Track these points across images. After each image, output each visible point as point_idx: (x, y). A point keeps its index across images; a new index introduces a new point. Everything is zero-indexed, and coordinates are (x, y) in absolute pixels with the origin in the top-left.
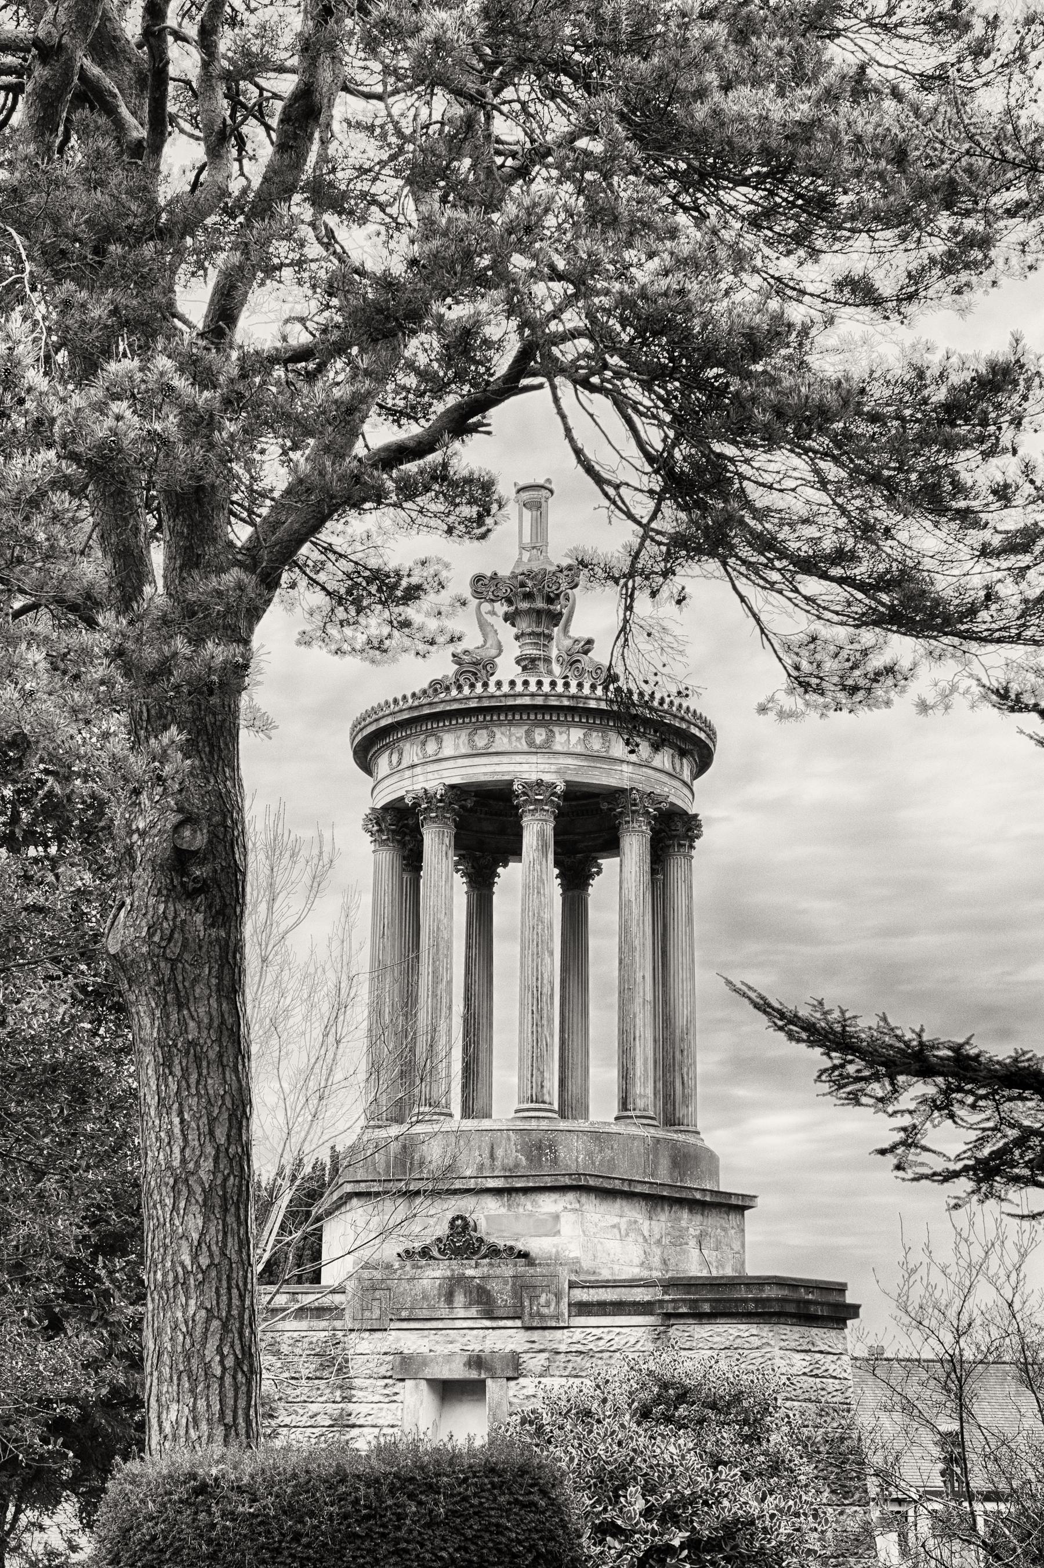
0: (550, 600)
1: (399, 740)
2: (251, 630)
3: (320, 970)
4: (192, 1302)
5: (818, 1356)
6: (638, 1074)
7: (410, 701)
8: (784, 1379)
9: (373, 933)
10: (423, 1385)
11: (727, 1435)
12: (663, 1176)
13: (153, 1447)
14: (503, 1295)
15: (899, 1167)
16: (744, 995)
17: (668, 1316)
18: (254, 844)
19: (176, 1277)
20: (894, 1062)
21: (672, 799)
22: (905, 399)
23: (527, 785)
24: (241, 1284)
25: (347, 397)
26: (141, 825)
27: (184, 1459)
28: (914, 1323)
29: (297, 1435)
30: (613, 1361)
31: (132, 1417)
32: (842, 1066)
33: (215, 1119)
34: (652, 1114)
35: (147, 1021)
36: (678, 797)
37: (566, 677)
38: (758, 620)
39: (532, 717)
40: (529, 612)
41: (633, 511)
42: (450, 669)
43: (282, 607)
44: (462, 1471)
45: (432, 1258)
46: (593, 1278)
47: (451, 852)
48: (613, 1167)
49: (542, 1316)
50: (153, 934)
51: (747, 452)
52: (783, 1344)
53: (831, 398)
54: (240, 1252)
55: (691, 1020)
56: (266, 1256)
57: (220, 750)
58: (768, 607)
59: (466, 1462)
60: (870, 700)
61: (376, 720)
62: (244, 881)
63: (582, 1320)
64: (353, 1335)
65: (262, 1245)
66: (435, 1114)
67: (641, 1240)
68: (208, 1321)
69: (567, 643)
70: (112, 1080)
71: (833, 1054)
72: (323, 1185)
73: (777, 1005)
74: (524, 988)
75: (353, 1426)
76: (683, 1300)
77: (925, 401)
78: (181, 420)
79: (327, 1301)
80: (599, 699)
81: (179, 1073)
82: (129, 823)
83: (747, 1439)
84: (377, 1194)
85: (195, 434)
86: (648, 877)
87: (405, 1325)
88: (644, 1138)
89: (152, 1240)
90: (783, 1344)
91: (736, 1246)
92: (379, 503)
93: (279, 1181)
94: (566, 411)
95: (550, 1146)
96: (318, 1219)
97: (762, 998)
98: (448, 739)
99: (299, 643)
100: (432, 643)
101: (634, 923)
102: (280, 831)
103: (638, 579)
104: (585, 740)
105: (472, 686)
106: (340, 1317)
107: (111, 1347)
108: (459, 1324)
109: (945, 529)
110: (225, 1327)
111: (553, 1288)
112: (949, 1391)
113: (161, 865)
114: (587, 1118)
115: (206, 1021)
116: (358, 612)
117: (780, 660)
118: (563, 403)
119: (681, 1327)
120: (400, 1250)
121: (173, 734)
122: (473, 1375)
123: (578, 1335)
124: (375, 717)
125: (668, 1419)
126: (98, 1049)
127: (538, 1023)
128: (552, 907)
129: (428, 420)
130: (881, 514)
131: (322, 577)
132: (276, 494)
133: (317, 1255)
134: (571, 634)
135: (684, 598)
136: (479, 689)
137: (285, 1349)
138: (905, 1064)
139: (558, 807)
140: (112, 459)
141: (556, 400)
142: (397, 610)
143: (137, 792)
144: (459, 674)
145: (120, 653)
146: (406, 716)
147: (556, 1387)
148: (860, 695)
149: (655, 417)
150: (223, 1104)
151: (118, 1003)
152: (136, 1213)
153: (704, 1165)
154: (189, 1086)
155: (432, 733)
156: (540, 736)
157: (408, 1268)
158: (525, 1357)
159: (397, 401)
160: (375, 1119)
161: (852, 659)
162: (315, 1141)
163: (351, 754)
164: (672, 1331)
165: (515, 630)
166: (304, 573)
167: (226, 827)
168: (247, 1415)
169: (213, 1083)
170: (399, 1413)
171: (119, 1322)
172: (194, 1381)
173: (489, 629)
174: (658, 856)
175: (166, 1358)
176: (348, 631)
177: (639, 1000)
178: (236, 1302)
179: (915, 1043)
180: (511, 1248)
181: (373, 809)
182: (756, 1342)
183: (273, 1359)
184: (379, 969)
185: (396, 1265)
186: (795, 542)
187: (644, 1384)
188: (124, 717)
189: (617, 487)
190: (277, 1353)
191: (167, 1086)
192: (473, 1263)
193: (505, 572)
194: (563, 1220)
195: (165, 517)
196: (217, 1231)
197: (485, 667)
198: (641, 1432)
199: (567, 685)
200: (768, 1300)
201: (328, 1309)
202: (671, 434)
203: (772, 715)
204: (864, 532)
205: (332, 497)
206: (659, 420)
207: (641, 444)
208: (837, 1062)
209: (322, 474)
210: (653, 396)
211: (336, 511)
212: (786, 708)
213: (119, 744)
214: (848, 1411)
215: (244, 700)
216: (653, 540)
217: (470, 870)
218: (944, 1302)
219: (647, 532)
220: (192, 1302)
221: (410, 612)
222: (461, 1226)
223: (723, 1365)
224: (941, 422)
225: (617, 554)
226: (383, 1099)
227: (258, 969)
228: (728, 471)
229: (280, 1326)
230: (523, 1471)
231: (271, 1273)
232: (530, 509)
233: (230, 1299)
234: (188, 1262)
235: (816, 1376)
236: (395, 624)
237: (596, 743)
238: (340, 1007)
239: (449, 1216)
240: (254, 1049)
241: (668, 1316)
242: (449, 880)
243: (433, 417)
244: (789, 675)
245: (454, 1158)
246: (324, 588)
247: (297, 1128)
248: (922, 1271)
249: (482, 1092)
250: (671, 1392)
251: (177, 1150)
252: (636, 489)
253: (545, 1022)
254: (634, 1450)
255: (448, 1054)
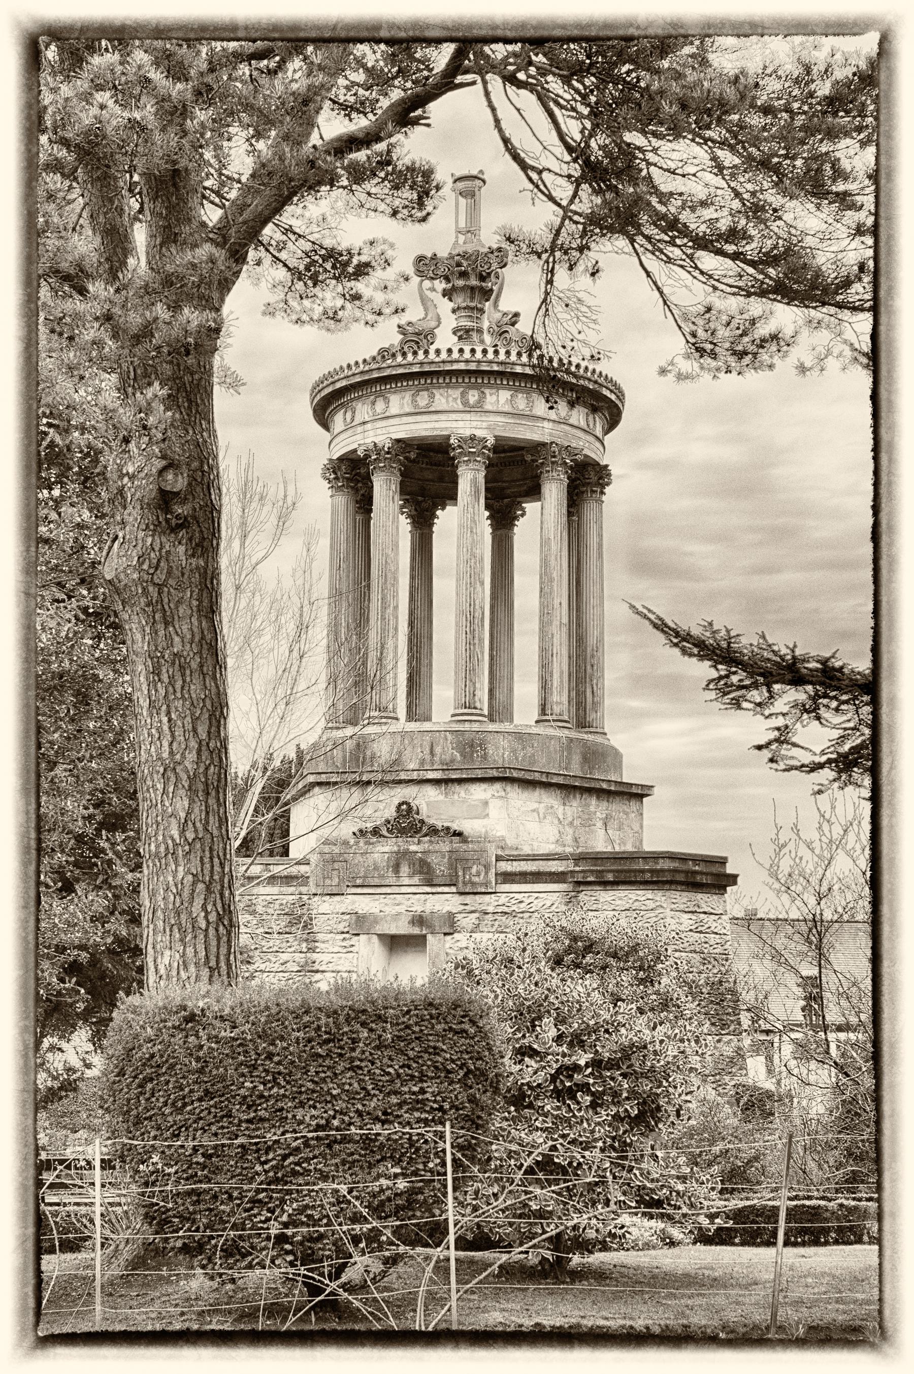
0: (482, 278)
1: (352, 400)
2: (222, 300)
3: (286, 597)
4: (181, 869)
5: (702, 916)
6: (555, 685)
7: (362, 366)
8: (674, 934)
9: (331, 565)
10: (375, 939)
11: (626, 978)
12: (576, 769)
13: (151, 985)
14: (440, 865)
15: (772, 760)
16: (645, 617)
17: (579, 883)
18: (228, 490)
19: (167, 848)
20: (771, 673)
21: (586, 452)
22: (794, 94)
23: (462, 439)
24: (221, 854)
25: (303, 90)
26: (131, 470)
27: (176, 995)
28: (783, 889)
29: (269, 979)
30: (532, 920)
31: (133, 962)
32: (727, 676)
33: (197, 718)
34: (566, 718)
35: (138, 636)
36: (591, 450)
37: (496, 346)
38: (661, 293)
39: (467, 380)
40: (463, 289)
41: (554, 194)
42: (396, 339)
43: (249, 282)
44: (405, 1005)
45: (381, 836)
46: (515, 853)
47: (397, 497)
48: (533, 763)
49: (473, 884)
50: (143, 563)
51: (655, 142)
52: (673, 906)
53: (730, 93)
54: (220, 827)
55: (601, 640)
56: (243, 834)
57: (197, 405)
58: (670, 282)
59: (409, 998)
60: (755, 365)
61: (333, 383)
62: (219, 518)
63: (507, 887)
64: (316, 898)
65: (239, 824)
66: (382, 717)
67: (556, 822)
68: (194, 884)
69: (498, 316)
70: (110, 686)
71: (720, 667)
72: (290, 776)
73: (673, 625)
74: (460, 613)
75: (317, 971)
76: (592, 871)
77: (811, 95)
78: (158, 110)
79: (294, 870)
80: (524, 365)
81: (166, 680)
82: (120, 468)
83: (642, 981)
84: (335, 783)
85: (170, 122)
86: (565, 519)
87: (359, 890)
88: (560, 738)
89: (147, 818)
90: (673, 906)
91: (636, 827)
92: (332, 185)
93: (253, 772)
94: (496, 104)
95: (480, 745)
96: (286, 804)
97: (661, 619)
98: (394, 399)
99: (264, 314)
100: (380, 314)
101: (553, 557)
102: (250, 478)
103: (558, 254)
104: (511, 401)
105: (415, 353)
106: (305, 884)
107: (114, 905)
108: (404, 890)
109: (826, 210)
110: (208, 889)
111: (483, 861)
112: (811, 943)
113: (148, 504)
114: (511, 721)
115: (189, 636)
116: (315, 285)
117: (680, 328)
118: (493, 97)
119: (589, 893)
120: (355, 830)
121: (156, 390)
122: (416, 931)
123: (503, 899)
124: (331, 380)
125: (577, 966)
126: (97, 660)
127: (471, 642)
128: (483, 543)
129: (375, 114)
130: (773, 198)
131: (283, 255)
132: (244, 179)
133: (286, 833)
134: (500, 308)
135: (598, 271)
136: (421, 356)
137: (260, 909)
138: (779, 674)
139: (488, 458)
140: (97, 144)
141: (487, 94)
142: (349, 285)
143: (126, 440)
144: (403, 342)
145: (108, 318)
146: (358, 379)
147: (484, 940)
148: (747, 360)
149: (573, 109)
150: (204, 706)
151: (114, 622)
152: (133, 796)
153: (609, 759)
154: (175, 691)
155: (381, 394)
156: (473, 396)
157: (361, 844)
158: (459, 916)
159: (348, 97)
160: (333, 722)
161: (742, 327)
162: (283, 738)
163: (311, 412)
164: (582, 896)
165: (451, 305)
166: (267, 250)
167: (203, 472)
168: (228, 960)
169: (195, 689)
170: (355, 961)
171: (121, 886)
172: (183, 932)
173: (429, 303)
174: (574, 501)
175: (159, 913)
176: (306, 303)
177: (556, 623)
178: (217, 868)
179: (789, 657)
180: (448, 828)
181: (330, 460)
182: (651, 904)
183: (250, 918)
184: (336, 595)
185: (352, 842)
186: (695, 222)
187: (557, 938)
188: (114, 377)
189: (540, 172)
190: (253, 913)
191: (156, 690)
192: (416, 840)
193: (443, 253)
194: (491, 805)
195: (146, 200)
196: (201, 811)
197: (426, 337)
198: (554, 975)
199: (496, 352)
200: (662, 871)
201: (296, 877)
202: (588, 125)
203: (671, 377)
204: (755, 213)
205: (291, 180)
206: (577, 112)
207: (561, 136)
208: (723, 673)
209: (282, 159)
210: (572, 92)
211: (295, 194)
212: (683, 371)
213: (110, 397)
214: (727, 960)
215: (217, 360)
216: (571, 219)
217: (414, 513)
218: (808, 871)
219: (567, 214)
220: (181, 869)
221: (360, 286)
222: (406, 810)
223: (623, 922)
224: (824, 113)
225: (539, 232)
226: (340, 706)
227: (233, 596)
228: (637, 158)
229: (255, 891)
230: (456, 1006)
231: (247, 847)
232: (465, 197)
233: (212, 867)
234: (177, 837)
235: (701, 932)
236: (347, 297)
237: (521, 402)
238: (302, 628)
239: (396, 802)
240: (230, 662)
241: (579, 883)
242: (395, 521)
243: (379, 112)
244: (688, 342)
245: (400, 754)
246: (285, 265)
247: (268, 729)
248: (791, 846)
249: (424, 701)
250: (580, 944)
251: (166, 744)
252: (556, 174)
253: (476, 641)
254: (548, 990)
255: (395, 666)
